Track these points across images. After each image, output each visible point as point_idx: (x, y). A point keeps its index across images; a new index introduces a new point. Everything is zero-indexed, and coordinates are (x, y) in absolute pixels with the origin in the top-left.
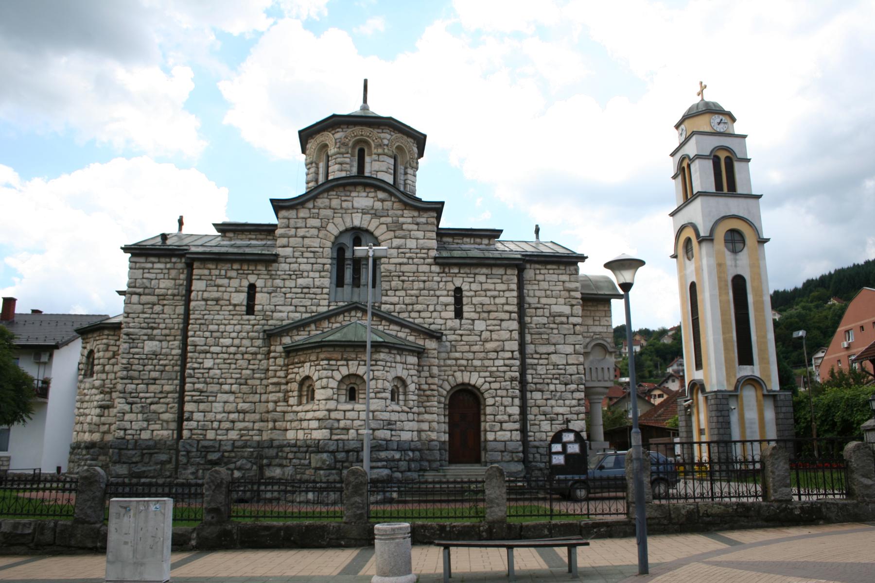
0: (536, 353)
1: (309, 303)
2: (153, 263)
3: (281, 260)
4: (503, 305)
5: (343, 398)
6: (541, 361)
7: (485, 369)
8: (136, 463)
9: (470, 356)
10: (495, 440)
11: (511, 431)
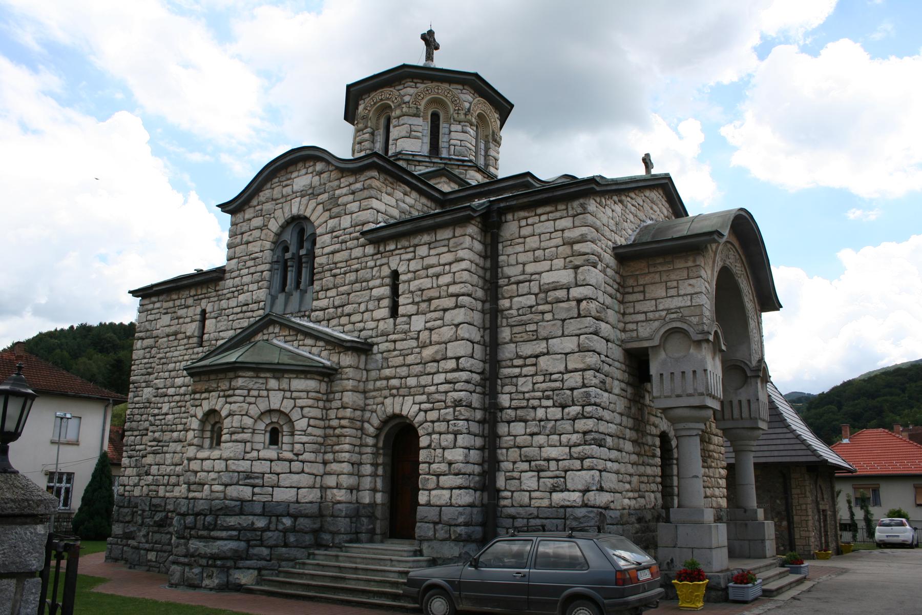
3: (227, 275)
4: (448, 285)
5: (207, 442)
6: (525, 370)
7: (421, 390)
9: (403, 371)
10: (428, 504)
11: (451, 489)
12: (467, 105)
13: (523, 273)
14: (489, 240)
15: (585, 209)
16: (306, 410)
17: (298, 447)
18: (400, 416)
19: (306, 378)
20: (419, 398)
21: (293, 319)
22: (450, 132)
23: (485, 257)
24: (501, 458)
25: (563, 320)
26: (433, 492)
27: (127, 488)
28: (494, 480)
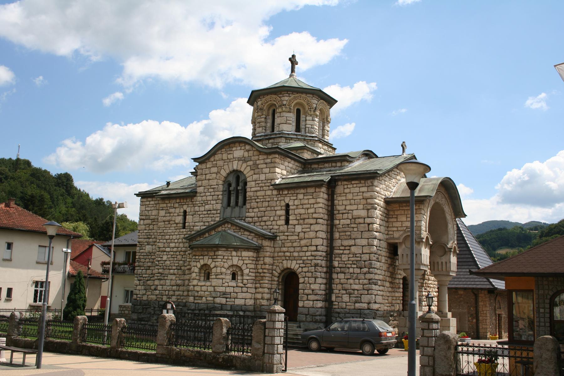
0: (342, 246)
1: (210, 220)
2: (150, 201)
3: (198, 195)
4: (312, 214)
5: (202, 278)
6: (346, 252)
7: (300, 258)
8: (140, 313)
9: (292, 249)
10: (303, 307)
11: (313, 301)
12: (315, 106)
13: (345, 209)
14: (330, 193)
15: (373, 184)
16: (248, 265)
17: (245, 281)
18: (290, 269)
19: (248, 251)
20: (299, 262)
21: (236, 221)
22: (306, 120)
23: (328, 200)
24: (334, 288)
25: (362, 232)
26: (305, 302)
27: (138, 296)
28: (330, 297)
